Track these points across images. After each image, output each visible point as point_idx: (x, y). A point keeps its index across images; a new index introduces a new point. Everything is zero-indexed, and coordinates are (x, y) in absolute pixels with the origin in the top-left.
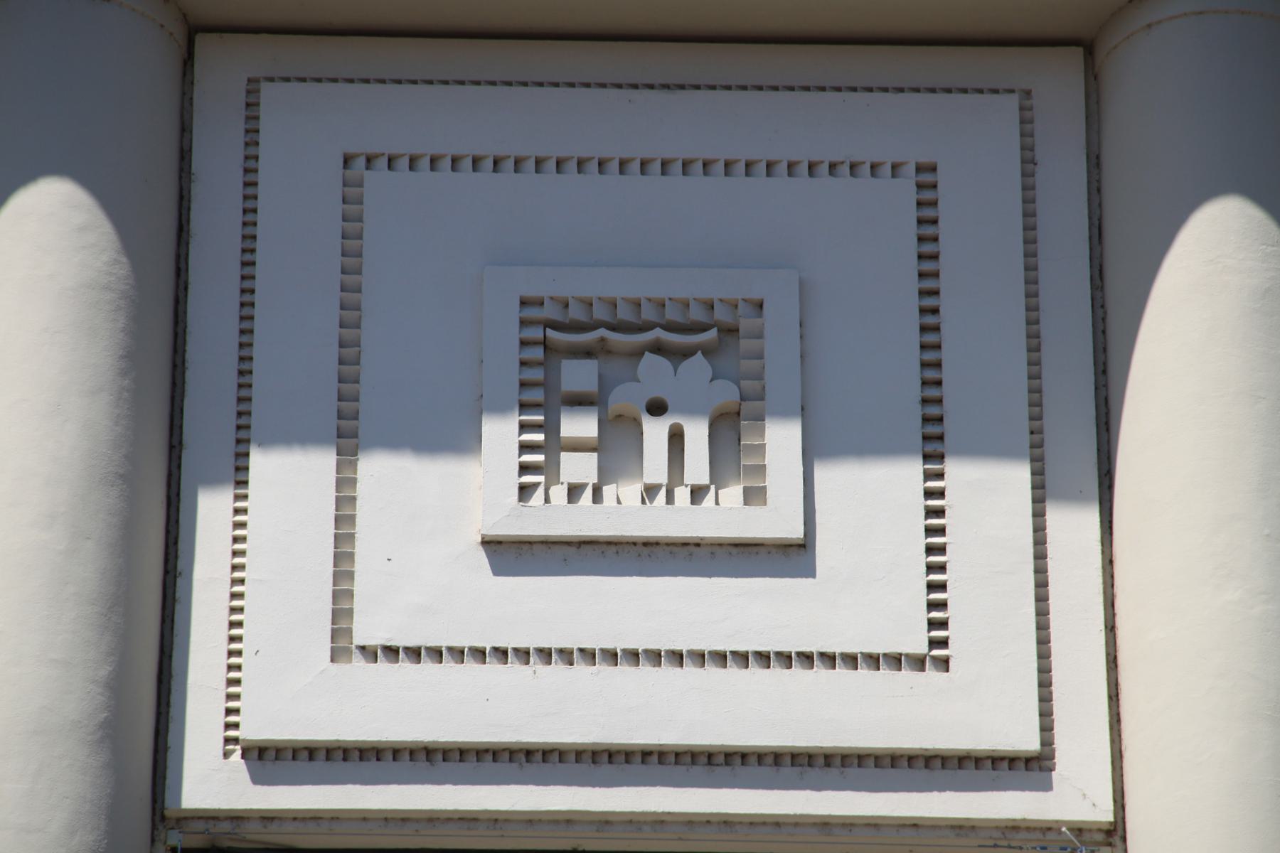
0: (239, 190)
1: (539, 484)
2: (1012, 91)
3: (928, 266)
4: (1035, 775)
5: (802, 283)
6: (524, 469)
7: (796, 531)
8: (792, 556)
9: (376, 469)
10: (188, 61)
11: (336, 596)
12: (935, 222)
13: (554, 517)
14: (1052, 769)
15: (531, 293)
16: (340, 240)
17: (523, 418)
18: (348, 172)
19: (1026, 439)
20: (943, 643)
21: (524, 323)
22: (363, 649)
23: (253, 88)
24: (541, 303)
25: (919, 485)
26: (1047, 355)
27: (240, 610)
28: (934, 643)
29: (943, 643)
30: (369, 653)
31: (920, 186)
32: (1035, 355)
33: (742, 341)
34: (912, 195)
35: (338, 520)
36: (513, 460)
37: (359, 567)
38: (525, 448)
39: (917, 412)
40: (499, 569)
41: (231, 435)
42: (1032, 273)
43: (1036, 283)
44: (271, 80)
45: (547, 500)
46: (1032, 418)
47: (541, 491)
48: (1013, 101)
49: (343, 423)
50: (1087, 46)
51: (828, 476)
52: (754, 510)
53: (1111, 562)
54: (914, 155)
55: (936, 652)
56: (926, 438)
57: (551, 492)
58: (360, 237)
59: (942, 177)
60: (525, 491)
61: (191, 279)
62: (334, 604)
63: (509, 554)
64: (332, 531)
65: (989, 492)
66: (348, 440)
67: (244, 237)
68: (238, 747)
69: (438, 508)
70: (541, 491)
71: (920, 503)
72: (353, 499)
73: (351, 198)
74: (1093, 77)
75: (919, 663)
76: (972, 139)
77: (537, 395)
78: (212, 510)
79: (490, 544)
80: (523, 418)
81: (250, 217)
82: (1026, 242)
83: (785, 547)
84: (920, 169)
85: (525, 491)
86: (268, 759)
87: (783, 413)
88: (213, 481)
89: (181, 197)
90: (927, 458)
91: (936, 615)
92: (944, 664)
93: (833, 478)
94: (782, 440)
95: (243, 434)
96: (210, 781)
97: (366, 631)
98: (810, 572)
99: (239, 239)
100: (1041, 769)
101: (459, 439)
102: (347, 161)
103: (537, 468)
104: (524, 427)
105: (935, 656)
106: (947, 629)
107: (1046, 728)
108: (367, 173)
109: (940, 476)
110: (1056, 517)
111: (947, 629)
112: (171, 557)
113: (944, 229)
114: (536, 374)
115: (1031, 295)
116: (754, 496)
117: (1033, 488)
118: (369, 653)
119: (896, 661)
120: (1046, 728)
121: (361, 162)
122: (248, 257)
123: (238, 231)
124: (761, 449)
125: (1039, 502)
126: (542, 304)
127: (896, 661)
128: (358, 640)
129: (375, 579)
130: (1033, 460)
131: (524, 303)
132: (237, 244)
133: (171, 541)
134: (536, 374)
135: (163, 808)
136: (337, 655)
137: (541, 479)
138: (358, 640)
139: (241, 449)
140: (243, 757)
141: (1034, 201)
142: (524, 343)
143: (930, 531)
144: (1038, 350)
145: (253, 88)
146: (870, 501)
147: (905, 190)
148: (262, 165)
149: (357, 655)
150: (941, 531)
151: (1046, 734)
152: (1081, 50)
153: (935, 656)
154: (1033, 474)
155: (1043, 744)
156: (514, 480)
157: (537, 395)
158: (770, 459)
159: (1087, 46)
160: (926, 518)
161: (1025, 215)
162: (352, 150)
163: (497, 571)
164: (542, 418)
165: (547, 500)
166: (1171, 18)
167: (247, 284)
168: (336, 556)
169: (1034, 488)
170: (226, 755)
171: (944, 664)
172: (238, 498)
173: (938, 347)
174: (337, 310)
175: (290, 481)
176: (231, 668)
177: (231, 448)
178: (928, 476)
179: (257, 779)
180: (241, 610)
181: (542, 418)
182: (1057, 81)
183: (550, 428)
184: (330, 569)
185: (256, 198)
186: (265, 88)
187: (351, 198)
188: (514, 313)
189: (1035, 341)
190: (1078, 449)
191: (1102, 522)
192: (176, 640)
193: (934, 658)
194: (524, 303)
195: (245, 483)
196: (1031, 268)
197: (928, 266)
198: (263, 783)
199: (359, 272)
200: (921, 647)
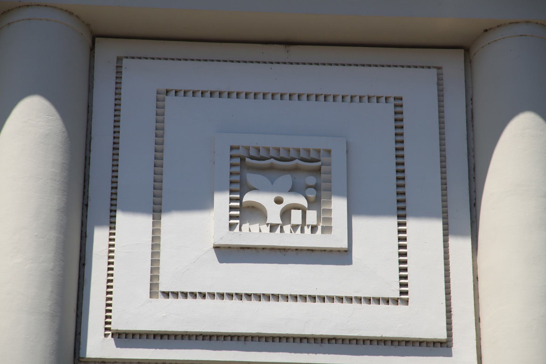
0: (112, 113)
1: (237, 224)
3: (399, 146)
4: (445, 349)
5: (347, 144)
6: (231, 217)
8: (342, 256)
9: (171, 221)
10: (92, 49)
11: (153, 246)
12: (402, 120)
14: (451, 347)
15: (235, 144)
17: (231, 196)
20: (406, 293)
22: (163, 293)
23: (119, 59)
24: (238, 148)
25: (396, 228)
26: (449, 170)
27: (112, 275)
28: (402, 293)
29: (406, 293)
30: (166, 294)
31: (396, 106)
33: (322, 175)
37: (162, 265)
38: (232, 208)
41: (108, 207)
43: (445, 167)
44: (127, 58)
45: (240, 230)
47: (238, 226)
51: (358, 222)
52: (326, 235)
54: (393, 93)
55: (403, 297)
56: (399, 209)
57: (242, 227)
59: (404, 102)
61: (90, 196)
63: (226, 253)
64: (151, 235)
65: (425, 232)
67: (113, 177)
69: (195, 233)
70: (238, 226)
71: (397, 258)
73: (160, 114)
74: (468, 62)
75: (396, 301)
76: (416, 87)
77: (237, 187)
78: (100, 236)
80: (231, 196)
81: (116, 129)
83: (339, 251)
85: (232, 227)
86: (123, 337)
87: (339, 194)
88: (101, 224)
89: (88, 106)
90: (399, 217)
91: (403, 281)
92: (406, 302)
93: (360, 223)
94: (339, 206)
95: (113, 208)
96: (97, 345)
98: (349, 262)
100: (447, 347)
101: (204, 203)
104: (231, 200)
105: (402, 298)
107: (449, 329)
108: (166, 97)
109: (405, 224)
110: (453, 242)
112: (87, 165)
113: (406, 145)
114: (236, 178)
115: (443, 178)
116: (327, 229)
118: (166, 294)
119: (387, 301)
120: (449, 329)
122: (115, 168)
123: (110, 174)
124: (330, 211)
125: (446, 236)
126: (239, 148)
127: (387, 301)
129: (167, 260)
130: (444, 218)
131: (232, 148)
132: (110, 168)
133: (84, 235)
134: (236, 178)
135: (79, 353)
136: (153, 294)
137: (238, 221)
138: (162, 288)
142: (232, 165)
143: (401, 270)
144: (446, 190)
145: (119, 59)
146: (375, 234)
147: (390, 108)
148: (122, 108)
150: (405, 262)
151: (449, 332)
152: (463, 51)
153: (402, 298)
154: (443, 224)
156: (227, 222)
158: (334, 215)
161: (441, 151)
163: (221, 261)
164: (238, 196)
165: (240, 230)
167: (117, 102)
168: (152, 245)
169: (444, 230)
170: (106, 335)
171: (406, 302)
172: (111, 228)
173: (402, 142)
174: (154, 153)
175: (133, 226)
177: (108, 214)
178: (399, 224)
179: (118, 345)
180: (114, 240)
181: (238, 196)
182: (453, 65)
186: (125, 60)
187: (160, 114)
188: (228, 153)
189: (445, 186)
190: (463, 214)
192: (81, 347)
193: (401, 299)
194: (232, 148)
195: (114, 228)
196: (443, 167)
198: (121, 347)
200: (397, 295)
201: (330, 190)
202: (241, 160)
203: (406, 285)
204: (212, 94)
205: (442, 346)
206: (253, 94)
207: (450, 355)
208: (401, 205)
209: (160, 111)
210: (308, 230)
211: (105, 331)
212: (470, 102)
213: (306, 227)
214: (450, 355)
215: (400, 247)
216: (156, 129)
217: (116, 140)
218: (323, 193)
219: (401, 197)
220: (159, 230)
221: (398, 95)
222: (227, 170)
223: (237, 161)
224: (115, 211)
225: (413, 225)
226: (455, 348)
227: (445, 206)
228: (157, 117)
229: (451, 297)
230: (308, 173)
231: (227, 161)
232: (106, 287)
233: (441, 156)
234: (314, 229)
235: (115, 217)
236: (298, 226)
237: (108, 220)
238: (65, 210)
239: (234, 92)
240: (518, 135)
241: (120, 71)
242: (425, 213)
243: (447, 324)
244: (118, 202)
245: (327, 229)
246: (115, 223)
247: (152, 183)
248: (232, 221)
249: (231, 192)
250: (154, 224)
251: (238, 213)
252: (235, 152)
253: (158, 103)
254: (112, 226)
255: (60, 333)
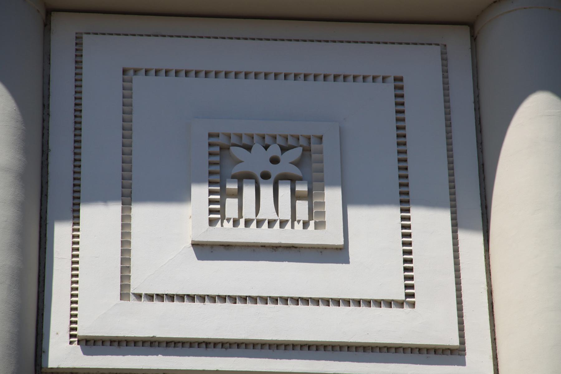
2: (438, 45)
6: (211, 211)
7: (340, 242)
8: (338, 254)
9: (141, 212)
10: (47, 25)
11: (123, 226)
13: (225, 233)
15: (214, 131)
16: (121, 131)
18: (125, 77)
19: (448, 197)
20: (413, 295)
21: (210, 145)
22: (135, 294)
24: (218, 136)
26: (458, 190)
28: (408, 295)
29: (413, 295)
31: (396, 88)
32: (453, 190)
34: (392, 92)
35: (123, 234)
36: (206, 207)
38: (211, 202)
39: (397, 181)
40: (200, 257)
42: (451, 159)
46: (451, 194)
48: (438, 48)
49: (125, 83)
50: (471, 25)
52: (318, 231)
53: (495, 339)
58: (131, 179)
59: (406, 83)
60: (212, 222)
62: (122, 238)
64: (120, 239)
65: (432, 223)
66: (127, 199)
68: (76, 339)
69: (170, 230)
72: (129, 277)
75: (400, 304)
76: (419, 64)
77: (216, 178)
78: (61, 232)
79: (195, 245)
82: (448, 150)
84: (396, 79)
85: (212, 222)
86: (90, 344)
87: (333, 184)
88: (62, 218)
90: (402, 211)
92: (413, 305)
93: (359, 215)
94: (332, 197)
96: (61, 352)
97: (136, 286)
99: (73, 105)
101: (181, 195)
102: (125, 71)
103: (217, 214)
104: (211, 192)
105: (409, 299)
106: (411, 246)
107: (462, 336)
109: (408, 211)
110: (462, 235)
111: (411, 246)
114: (216, 159)
116: (320, 225)
117: (452, 226)
118: (139, 296)
119: (389, 304)
120: (462, 336)
121: (132, 72)
124: (323, 204)
125: (455, 226)
127: (389, 304)
128: (132, 290)
131: (210, 135)
134: (216, 159)
136: (124, 296)
137: (219, 216)
138: (132, 290)
139: (76, 208)
140: (78, 344)
141: (451, 138)
143: (405, 261)
146: (374, 227)
147: (389, 88)
149: (132, 297)
153: (409, 299)
155: (460, 343)
156: (206, 217)
157: (216, 178)
158: (327, 209)
159: (471, 25)
160: (404, 264)
162: (127, 66)
166: (509, 12)
169: (452, 219)
170: (71, 343)
171: (413, 305)
172: (74, 224)
175: (99, 219)
176: (73, 289)
179: (85, 353)
183: (223, 187)
184: (119, 265)
185: (81, 80)
188: (206, 141)
190: (474, 207)
191: (484, 240)
194: (210, 135)
197: (402, 148)
199: (131, 179)
200: (403, 297)
201: (322, 180)
202: (221, 149)
203: (411, 270)
204: (187, 73)
205: (453, 354)
206: (233, 73)
207: (463, 364)
208: (400, 100)
209: (127, 133)
210: (299, 226)
211: (73, 232)
212: (485, 209)
213: (296, 223)
214: (463, 364)
215: (405, 261)
216: (123, 179)
217: (77, 176)
218: (315, 184)
219: (403, 173)
220: (129, 234)
221: (399, 75)
222: (206, 159)
223: (216, 149)
224: (79, 204)
225: (418, 215)
226: (469, 356)
227: (453, 194)
228: (124, 156)
229: (461, 287)
230: (300, 165)
231: (206, 150)
232: (70, 289)
233: (445, 107)
234: (306, 225)
235: (79, 211)
236: (287, 221)
237: (71, 214)
238: (22, 207)
239: (212, 71)
240: (533, 114)
241: (77, 222)
242: (431, 203)
243: (456, 277)
244: (82, 195)
245: (320, 225)
246: (79, 217)
247: (120, 115)
248: (212, 216)
249: (211, 183)
250: (123, 210)
251: (218, 197)
252: (213, 140)
253: (124, 181)
254: (76, 221)
255: (19, 315)
